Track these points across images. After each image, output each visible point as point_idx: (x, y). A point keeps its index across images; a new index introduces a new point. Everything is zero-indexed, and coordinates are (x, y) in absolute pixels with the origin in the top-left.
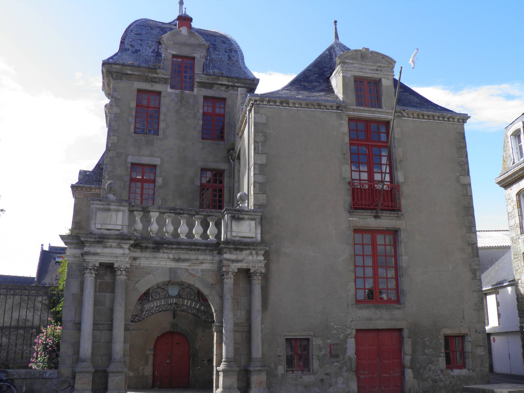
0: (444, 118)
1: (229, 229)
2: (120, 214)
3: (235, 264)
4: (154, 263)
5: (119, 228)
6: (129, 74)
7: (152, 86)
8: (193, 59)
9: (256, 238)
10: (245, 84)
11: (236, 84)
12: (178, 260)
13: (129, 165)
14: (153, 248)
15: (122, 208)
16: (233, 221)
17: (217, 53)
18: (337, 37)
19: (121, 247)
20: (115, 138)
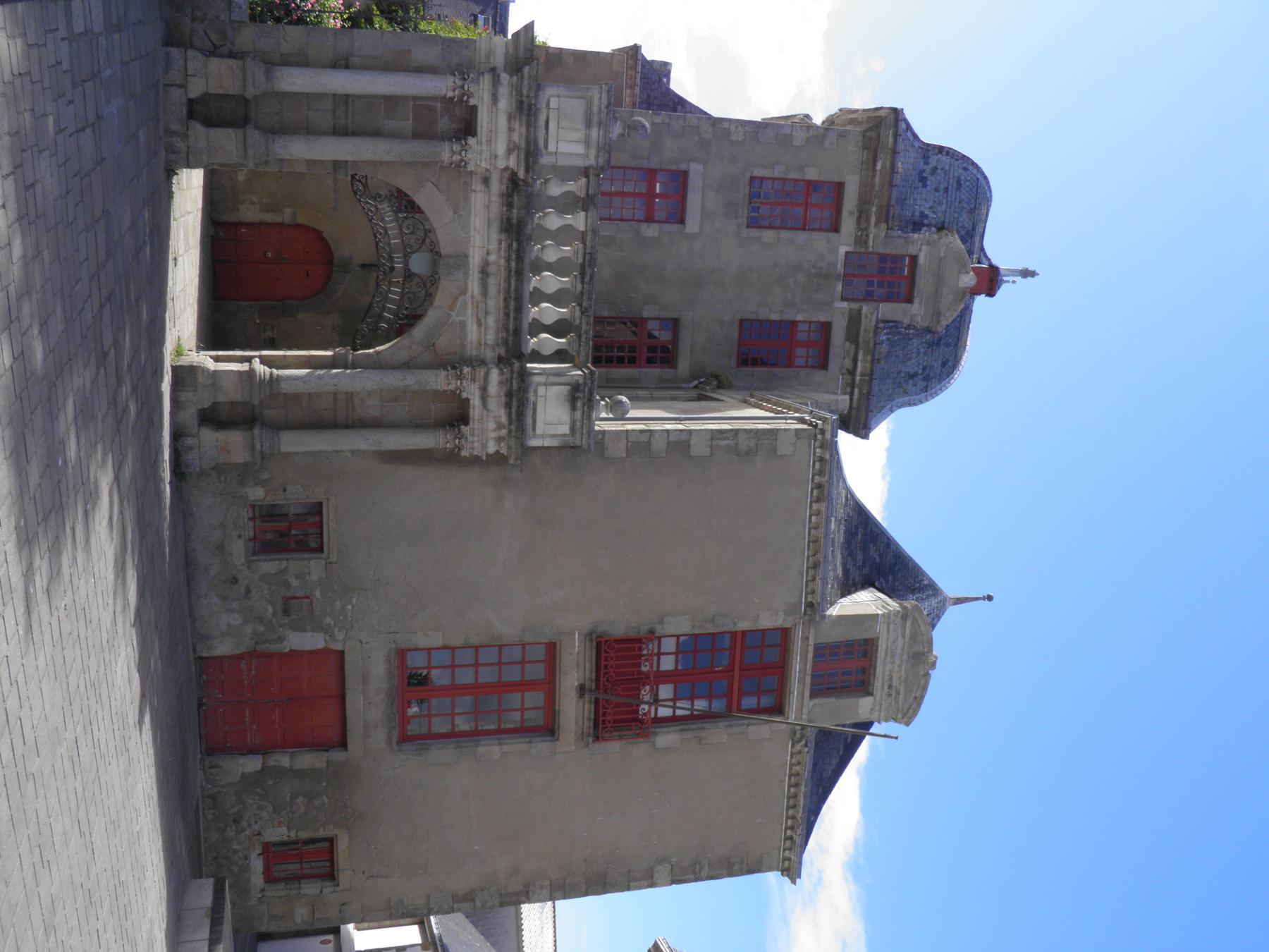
0: (792, 828)
1: (552, 379)
2: (580, 149)
4: (478, 221)
5: (552, 147)
6: (874, 165)
7: (851, 213)
8: (909, 300)
9: (535, 436)
10: (858, 408)
11: (856, 390)
12: (484, 272)
13: (683, 167)
14: (509, 220)
15: (593, 152)
16: (568, 388)
18: (959, 601)
19: (510, 151)
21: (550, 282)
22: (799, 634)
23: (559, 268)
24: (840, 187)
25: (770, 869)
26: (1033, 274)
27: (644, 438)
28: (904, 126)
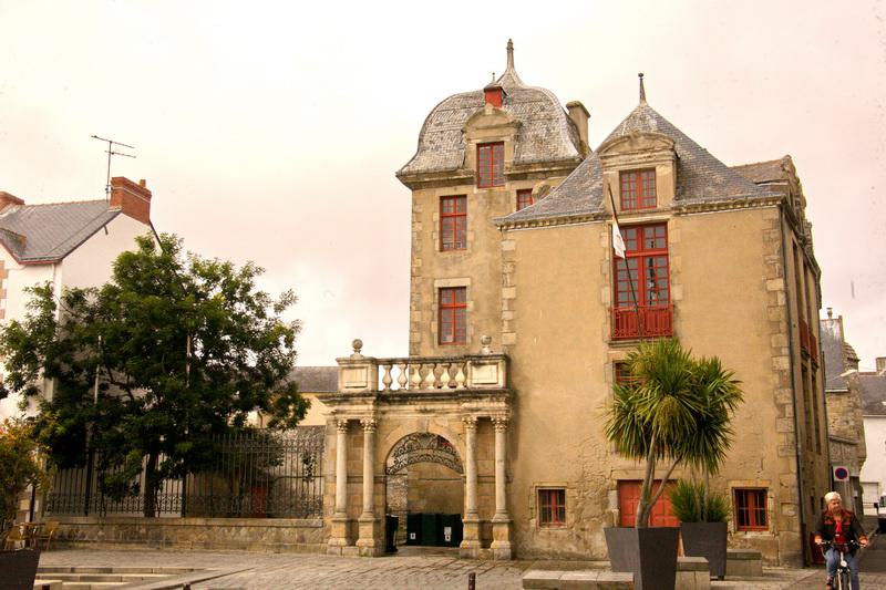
13: (437, 291)
18: (643, 96)
19: (366, 404)
21: (445, 377)
23: (423, 376)
24: (442, 198)
26: (510, 43)
28: (405, 170)
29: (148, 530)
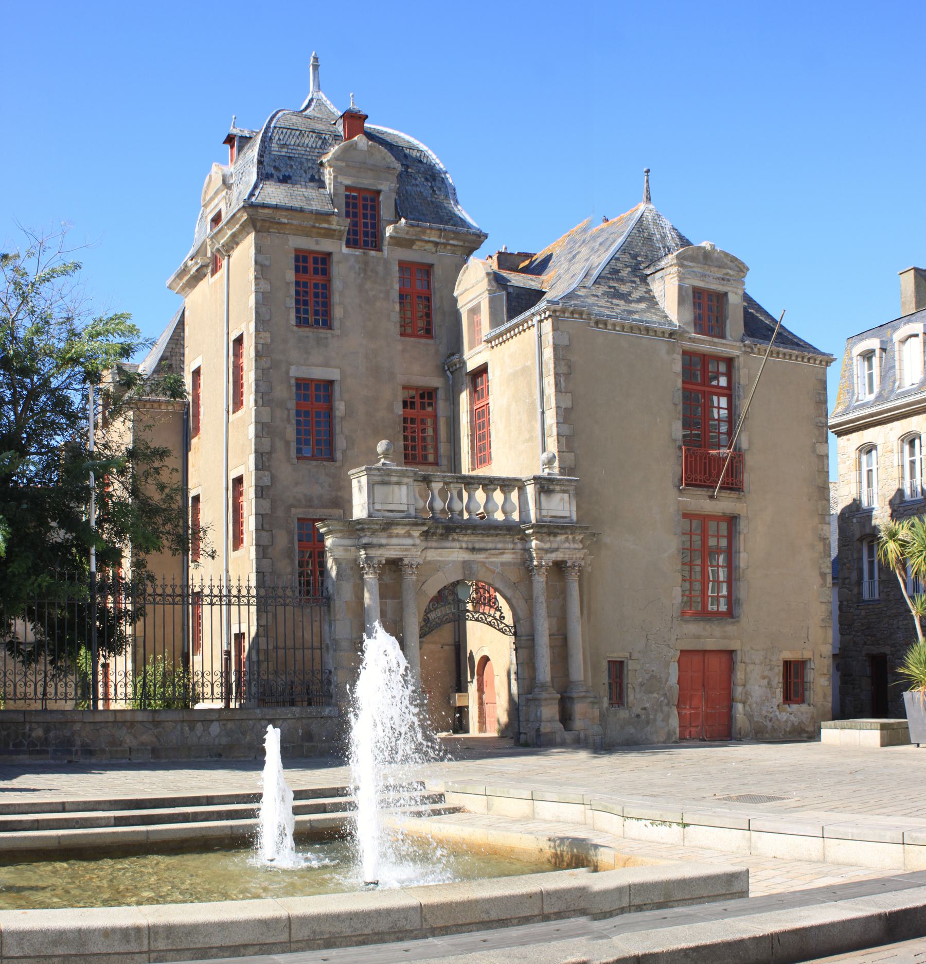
2: (404, 488)
3: (549, 555)
5: (404, 508)
6: (284, 224)
7: (317, 243)
9: (570, 517)
10: (464, 241)
11: (451, 242)
12: (473, 550)
13: (293, 382)
14: (442, 535)
16: (542, 494)
17: (413, 181)
20: (268, 335)
22: (688, 345)
25: (825, 374)
27: (563, 440)
29: (47, 731)
